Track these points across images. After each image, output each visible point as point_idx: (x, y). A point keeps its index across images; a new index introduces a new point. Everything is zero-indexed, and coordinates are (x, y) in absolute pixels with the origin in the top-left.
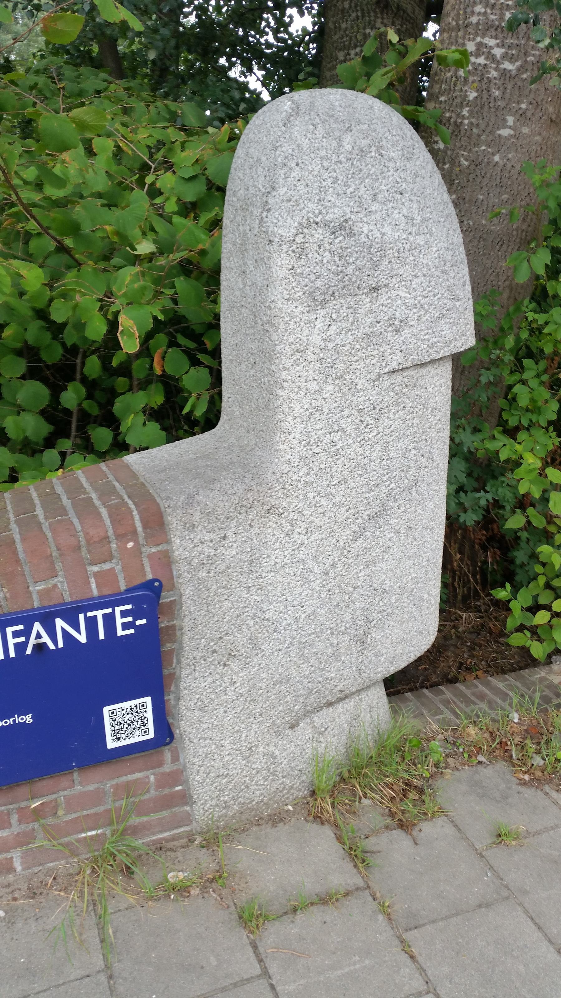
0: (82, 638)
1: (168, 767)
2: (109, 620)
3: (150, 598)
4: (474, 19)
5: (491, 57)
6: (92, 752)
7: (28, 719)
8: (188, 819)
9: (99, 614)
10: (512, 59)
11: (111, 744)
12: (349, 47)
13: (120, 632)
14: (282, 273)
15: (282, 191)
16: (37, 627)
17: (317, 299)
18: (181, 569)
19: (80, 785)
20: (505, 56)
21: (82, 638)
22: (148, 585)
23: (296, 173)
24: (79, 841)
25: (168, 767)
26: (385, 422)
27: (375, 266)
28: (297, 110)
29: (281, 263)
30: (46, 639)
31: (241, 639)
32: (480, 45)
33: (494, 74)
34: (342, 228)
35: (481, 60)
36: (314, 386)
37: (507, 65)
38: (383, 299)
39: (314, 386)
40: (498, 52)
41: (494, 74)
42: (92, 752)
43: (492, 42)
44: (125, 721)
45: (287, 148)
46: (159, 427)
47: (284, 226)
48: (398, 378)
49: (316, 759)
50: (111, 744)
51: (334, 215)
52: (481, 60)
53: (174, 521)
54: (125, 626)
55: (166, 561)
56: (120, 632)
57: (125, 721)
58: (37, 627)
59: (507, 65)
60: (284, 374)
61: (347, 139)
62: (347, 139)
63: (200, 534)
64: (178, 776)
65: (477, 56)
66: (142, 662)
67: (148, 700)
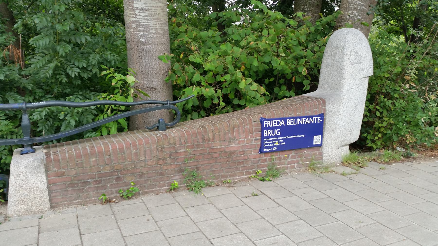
0: (313, 122)
1: (320, 151)
2: (317, 119)
3: (322, 116)
4: (351, 7)
5: (355, 15)
6: (311, 146)
7: (303, 136)
8: (322, 162)
9: (316, 118)
10: (360, 16)
11: (314, 144)
12: (305, 5)
13: (318, 122)
14: (347, 59)
15: (347, 46)
16: (307, 119)
17: (352, 64)
18: (327, 112)
19: (306, 152)
20: (358, 15)
21: (313, 122)
22: (322, 114)
23: (350, 43)
24: (305, 164)
25: (320, 151)
26: (360, 87)
27: (361, 59)
28: (348, 32)
29: (346, 58)
30: (308, 121)
31: (334, 127)
32: (352, 12)
33: (355, 19)
34: (356, 52)
35: (353, 16)
36: (350, 79)
37: (359, 17)
38: (361, 65)
39: (350, 79)
40: (357, 14)
41: (355, 19)
42: (311, 146)
43: (355, 12)
44: (317, 140)
45: (348, 39)
46: (371, 73)
47: (347, 51)
48: (362, 79)
49: (342, 156)
50: (314, 144)
51: (355, 50)
52: (353, 16)
53: (327, 103)
54: (319, 121)
55: (325, 110)
56: (318, 122)
57: (317, 140)
58: (307, 119)
59: (359, 17)
60: (345, 77)
61: (357, 37)
62: (357, 37)
63: (331, 106)
64: (321, 154)
65: (352, 14)
66: (319, 129)
67: (320, 136)
